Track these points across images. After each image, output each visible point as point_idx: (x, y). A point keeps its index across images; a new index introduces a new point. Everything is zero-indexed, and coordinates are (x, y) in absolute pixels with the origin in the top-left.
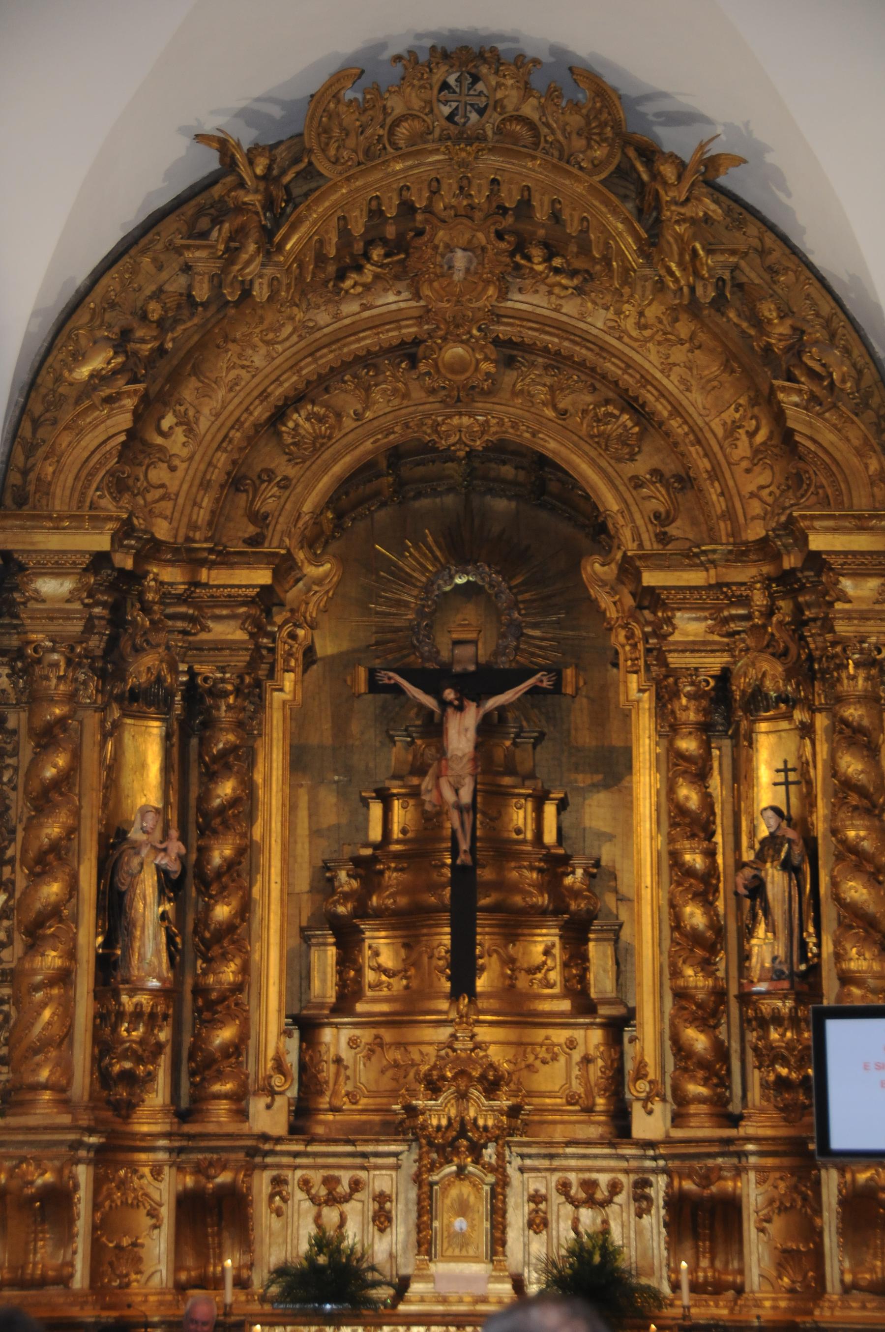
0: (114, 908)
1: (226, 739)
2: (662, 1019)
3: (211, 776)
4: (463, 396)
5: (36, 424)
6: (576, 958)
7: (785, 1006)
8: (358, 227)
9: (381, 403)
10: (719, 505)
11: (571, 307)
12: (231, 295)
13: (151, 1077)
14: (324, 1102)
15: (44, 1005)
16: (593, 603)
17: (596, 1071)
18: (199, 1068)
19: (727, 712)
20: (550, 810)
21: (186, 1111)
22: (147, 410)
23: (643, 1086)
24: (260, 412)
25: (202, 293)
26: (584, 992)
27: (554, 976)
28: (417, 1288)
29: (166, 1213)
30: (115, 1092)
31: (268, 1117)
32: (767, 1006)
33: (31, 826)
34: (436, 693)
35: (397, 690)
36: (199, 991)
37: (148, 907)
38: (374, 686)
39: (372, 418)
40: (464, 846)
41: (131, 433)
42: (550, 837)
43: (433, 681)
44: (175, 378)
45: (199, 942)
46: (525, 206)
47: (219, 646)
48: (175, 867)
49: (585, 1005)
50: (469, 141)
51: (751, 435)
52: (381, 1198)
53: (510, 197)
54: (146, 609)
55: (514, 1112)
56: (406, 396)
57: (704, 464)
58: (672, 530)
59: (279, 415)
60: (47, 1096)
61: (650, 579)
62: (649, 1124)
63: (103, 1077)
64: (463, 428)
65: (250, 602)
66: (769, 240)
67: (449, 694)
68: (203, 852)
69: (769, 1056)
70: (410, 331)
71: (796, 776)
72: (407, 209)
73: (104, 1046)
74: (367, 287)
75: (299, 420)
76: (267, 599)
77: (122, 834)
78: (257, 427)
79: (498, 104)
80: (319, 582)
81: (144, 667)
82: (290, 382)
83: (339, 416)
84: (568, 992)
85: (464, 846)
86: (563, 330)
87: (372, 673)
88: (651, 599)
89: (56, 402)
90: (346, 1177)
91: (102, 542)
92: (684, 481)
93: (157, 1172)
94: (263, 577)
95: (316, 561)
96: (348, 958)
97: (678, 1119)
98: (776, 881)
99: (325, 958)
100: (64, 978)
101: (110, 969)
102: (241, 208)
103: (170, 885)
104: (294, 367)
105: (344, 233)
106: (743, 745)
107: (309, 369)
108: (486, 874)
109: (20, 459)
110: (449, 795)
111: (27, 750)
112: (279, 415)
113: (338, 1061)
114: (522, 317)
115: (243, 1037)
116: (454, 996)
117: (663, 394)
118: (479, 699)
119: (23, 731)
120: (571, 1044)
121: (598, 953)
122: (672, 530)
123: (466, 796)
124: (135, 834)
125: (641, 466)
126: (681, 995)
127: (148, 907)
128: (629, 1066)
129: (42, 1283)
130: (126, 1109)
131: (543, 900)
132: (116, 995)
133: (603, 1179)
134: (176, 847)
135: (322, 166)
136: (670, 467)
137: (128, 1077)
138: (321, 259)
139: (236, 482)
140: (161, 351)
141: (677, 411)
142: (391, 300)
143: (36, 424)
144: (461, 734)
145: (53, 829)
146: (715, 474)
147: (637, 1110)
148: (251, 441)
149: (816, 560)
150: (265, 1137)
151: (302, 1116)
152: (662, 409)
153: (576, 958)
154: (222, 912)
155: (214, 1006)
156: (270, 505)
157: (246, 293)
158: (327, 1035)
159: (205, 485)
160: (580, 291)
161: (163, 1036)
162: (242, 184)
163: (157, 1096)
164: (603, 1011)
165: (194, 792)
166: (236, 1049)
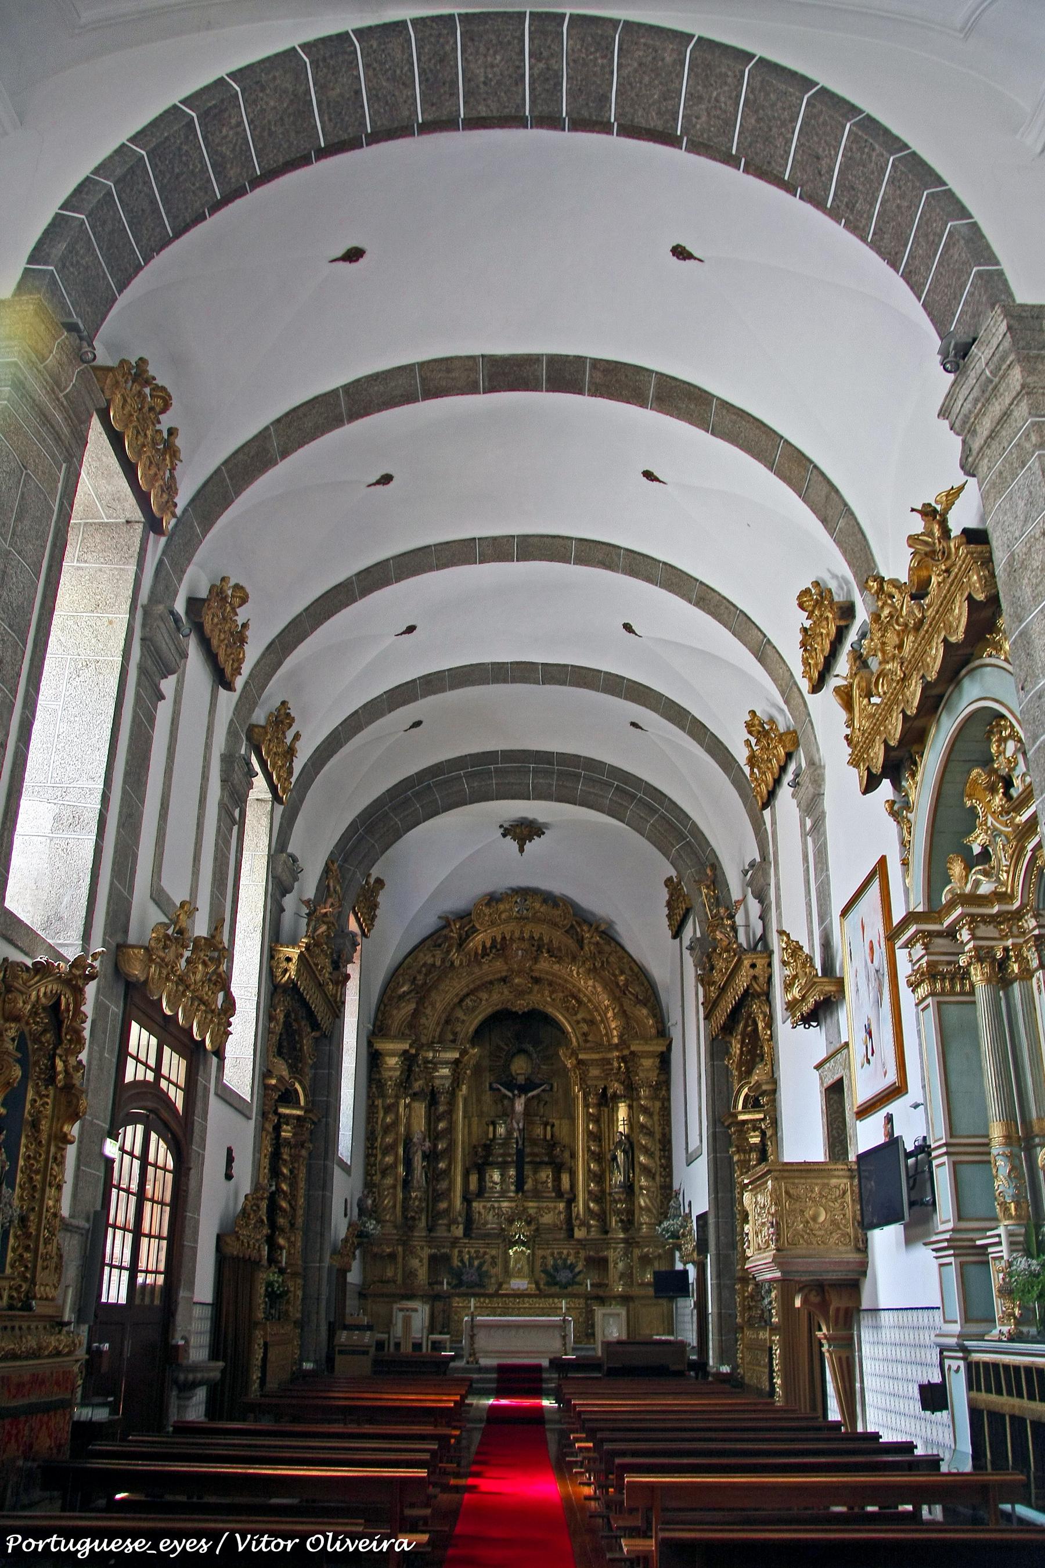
0: (408, 1163)
1: (441, 1109)
2: (23, 1316)
3: (439, 1119)
4: (520, 993)
5: (385, 1006)
6: (557, 1179)
7: (623, 1197)
8: (488, 945)
9: (495, 997)
10: (604, 1032)
11: (556, 967)
12: (448, 964)
13: (420, 1219)
14: (474, 1226)
15: (387, 1196)
16: (545, 1442)
17: (562, 1216)
18: (434, 1216)
19: (606, 1101)
20: (549, 1128)
21: (430, 1229)
22: (421, 1002)
23: (578, 1222)
24: (456, 1000)
25: (438, 963)
26: (560, 1190)
27: (550, 1185)
28: (505, 1286)
29: (426, 1261)
30: (408, 1224)
31: (459, 1231)
32: (617, 1197)
33: (396, 1141)
34: (512, 1092)
35: (499, 1089)
36: (434, 1190)
37: (418, 1161)
38: (491, 1088)
39: (491, 1002)
40: (520, 1143)
41: (415, 1010)
42: (549, 1137)
43: (510, 1086)
44: (429, 991)
45: (434, 1176)
46: (541, 939)
47: (442, 1077)
48: (428, 1151)
49: (560, 1194)
50: (524, 919)
51: (613, 1009)
52: (493, 1257)
53: (536, 936)
54: (419, 1066)
55: (537, 1230)
56: (502, 993)
57: (599, 1018)
58: (589, 1038)
59: (462, 1000)
60: (388, 1224)
61: (580, 1057)
62: (579, 1234)
63: (405, 1217)
64: (521, 1005)
65: (452, 1063)
66: (618, 948)
67: (516, 1092)
68: (435, 1146)
69: (618, 1212)
70: (504, 974)
71: (631, 1121)
72: (504, 938)
73: (405, 1209)
74: (490, 961)
75: (468, 1002)
76: (457, 1062)
77: (411, 1140)
78: (455, 1005)
79: (533, 908)
80: (474, 1055)
81: (417, 1085)
82: (465, 991)
83: (481, 1000)
84: (554, 1190)
85: (520, 1143)
86: (554, 975)
87: (490, 1084)
88: (580, 1062)
89: (391, 999)
90: (482, 1250)
91: (406, 1046)
92: (591, 1022)
93: (422, 1248)
94: (457, 1055)
95: (473, 1047)
96: (481, 1180)
97: (588, 1232)
98: (620, 1156)
99: (474, 1178)
100: (394, 1187)
101: (407, 1183)
102: (452, 938)
103: (425, 1156)
104: (467, 986)
105: (484, 946)
106: (614, 1110)
107: (472, 986)
108: (528, 1150)
109: (380, 1017)
110: (515, 1126)
111: (381, 1114)
112: (462, 1000)
113: (479, 1213)
114: (541, 971)
115: (449, 1206)
116: (517, 1192)
117: (585, 995)
118: (526, 1093)
119: (380, 1106)
120: (555, 1208)
121: (565, 1179)
122: (589, 1038)
123: (521, 1125)
124: (415, 1140)
125: (579, 1017)
126: (590, 1192)
127: (418, 1161)
128: (574, 1215)
129: (388, 1282)
130: (412, 1228)
131: (546, 1159)
132: (409, 1192)
133: (565, 1252)
134: (427, 1144)
135: (478, 926)
136: (588, 1017)
137: (413, 1218)
138: (476, 953)
139: (447, 1022)
140: (425, 983)
141: (590, 1000)
142: (499, 964)
143: (385, 1006)
144: (519, 1106)
145: (388, 1140)
146: (602, 1021)
147: (576, 1229)
148: (453, 1009)
149: (632, 1053)
150: (456, 1238)
151: (467, 1233)
152: (585, 999)
153: (557, 1179)
154: (442, 1165)
155: (438, 1196)
156: (458, 1029)
157: (452, 963)
158: (475, 1204)
159: (438, 1024)
160: (558, 962)
161: (424, 1205)
162: (452, 931)
163: (423, 1224)
164: (566, 1196)
165: (432, 1127)
166: (447, 1211)
